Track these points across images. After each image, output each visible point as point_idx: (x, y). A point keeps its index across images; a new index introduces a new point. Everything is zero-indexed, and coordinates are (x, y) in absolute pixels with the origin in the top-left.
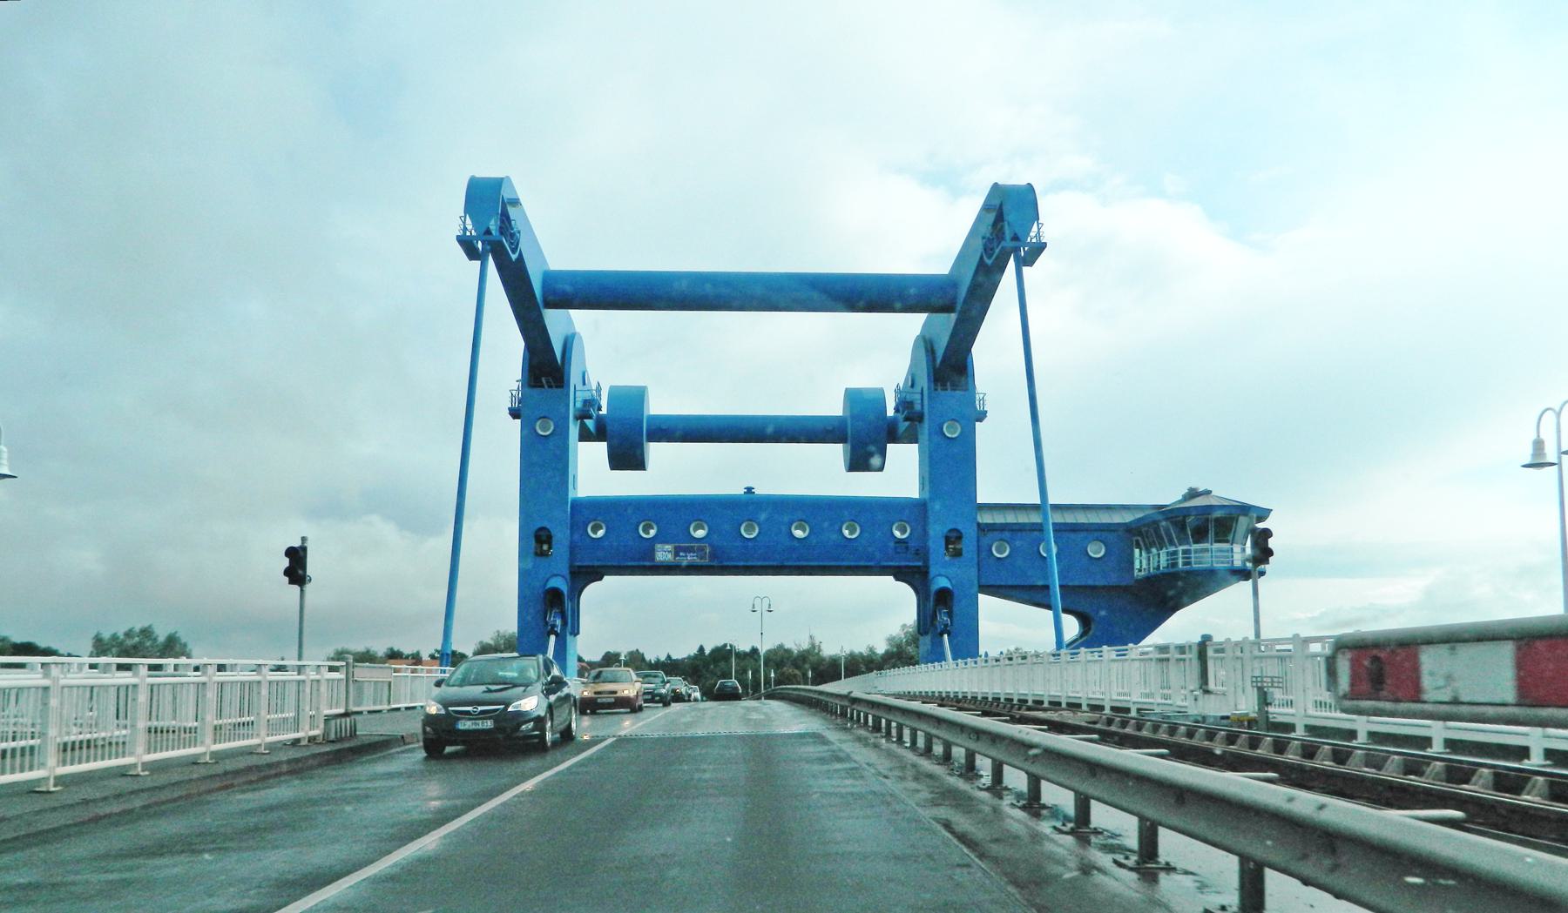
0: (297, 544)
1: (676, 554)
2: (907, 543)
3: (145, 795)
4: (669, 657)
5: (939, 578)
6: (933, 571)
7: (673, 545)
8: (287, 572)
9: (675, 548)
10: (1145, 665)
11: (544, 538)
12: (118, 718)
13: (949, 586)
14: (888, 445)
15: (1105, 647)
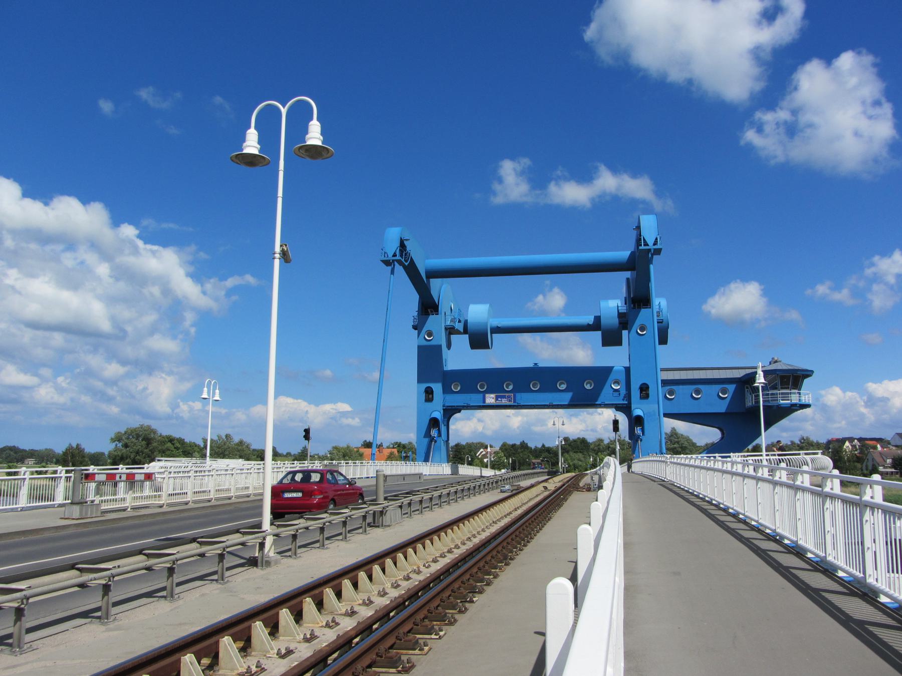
0: (307, 428)
1: (497, 399)
2: (619, 391)
3: (390, 671)
4: (543, 446)
5: (637, 410)
6: (633, 406)
7: (495, 395)
8: (304, 437)
9: (496, 396)
10: (661, 464)
11: (430, 392)
12: (889, 572)
13: (642, 415)
14: (623, 331)
15: (732, 453)
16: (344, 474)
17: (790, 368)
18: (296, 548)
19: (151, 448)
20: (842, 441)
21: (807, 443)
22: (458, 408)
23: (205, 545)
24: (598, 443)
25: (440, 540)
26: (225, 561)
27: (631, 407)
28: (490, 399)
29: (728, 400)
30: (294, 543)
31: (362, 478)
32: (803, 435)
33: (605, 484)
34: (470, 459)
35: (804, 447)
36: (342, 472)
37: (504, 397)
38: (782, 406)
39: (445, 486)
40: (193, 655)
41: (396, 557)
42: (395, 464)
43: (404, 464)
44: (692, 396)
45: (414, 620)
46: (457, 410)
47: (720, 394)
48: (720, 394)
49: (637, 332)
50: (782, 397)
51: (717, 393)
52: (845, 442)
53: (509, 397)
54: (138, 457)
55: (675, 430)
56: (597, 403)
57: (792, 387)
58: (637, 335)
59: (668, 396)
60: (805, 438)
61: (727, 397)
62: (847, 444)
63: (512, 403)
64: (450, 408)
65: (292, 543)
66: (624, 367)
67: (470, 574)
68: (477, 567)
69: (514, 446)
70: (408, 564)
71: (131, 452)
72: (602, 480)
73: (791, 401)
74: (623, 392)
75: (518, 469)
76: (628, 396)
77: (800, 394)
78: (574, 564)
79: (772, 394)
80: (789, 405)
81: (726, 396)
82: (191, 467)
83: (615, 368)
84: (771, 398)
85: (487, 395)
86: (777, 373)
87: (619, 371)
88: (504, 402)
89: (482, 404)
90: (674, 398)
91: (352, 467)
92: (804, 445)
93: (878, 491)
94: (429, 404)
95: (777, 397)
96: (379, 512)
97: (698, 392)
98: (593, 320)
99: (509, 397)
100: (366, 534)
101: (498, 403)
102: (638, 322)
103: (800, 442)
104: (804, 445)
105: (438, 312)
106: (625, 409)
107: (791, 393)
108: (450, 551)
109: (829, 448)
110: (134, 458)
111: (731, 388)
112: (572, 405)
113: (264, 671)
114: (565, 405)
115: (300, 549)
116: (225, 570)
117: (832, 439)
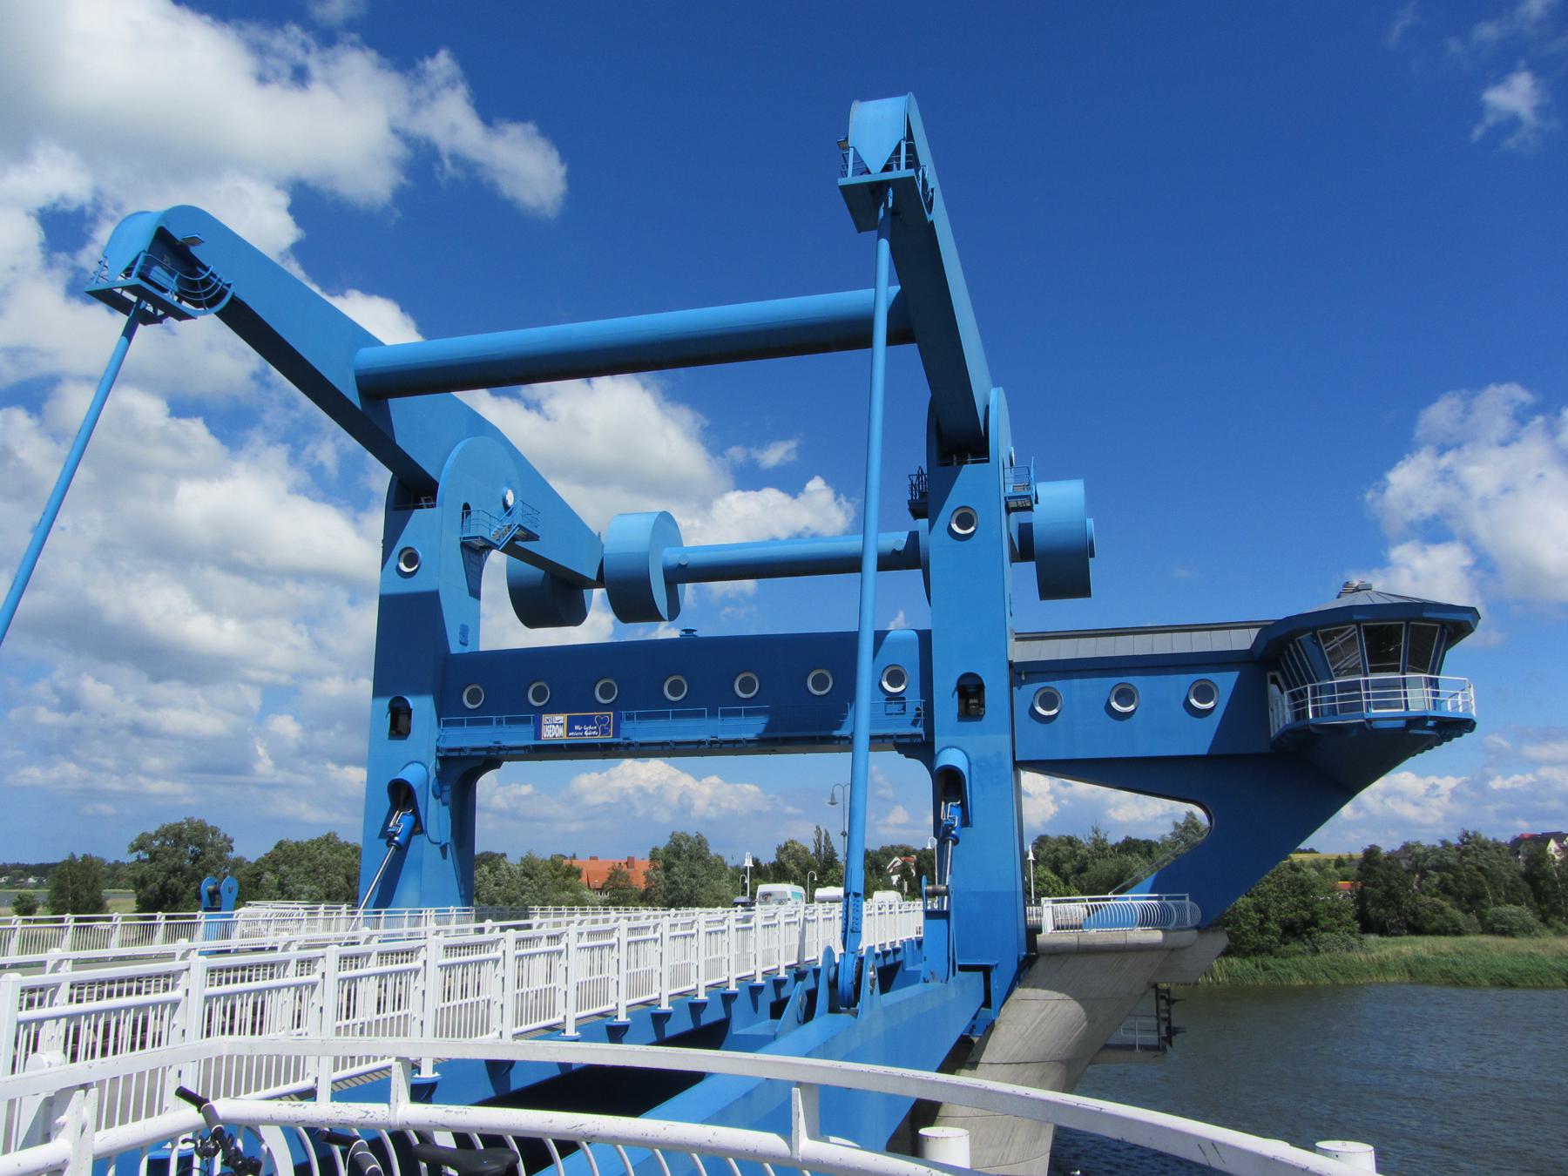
1: (570, 729)
13: (964, 769)
17: (1396, 600)
19: (201, 863)
20: (1545, 838)
21: (1477, 843)
22: (474, 753)
24: (1055, 846)
27: (933, 743)
28: (554, 728)
29: (1215, 720)
32: (1466, 829)
34: (816, 879)
35: (1471, 851)
37: (588, 721)
38: (1379, 725)
44: (1109, 708)
46: (491, 760)
47: (1193, 701)
48: (1193, 701)
49: (950, 530)
50: (1375, 696)
51: (1183, 699)
52: (1549, 841)
53: (602, 721)
54: (173, 880)
55: (1195, 818)
56: (836, 733)
57: (1410, 663)
58: (950, 539)
59: (1039, 709)
60: (1470, 834)
61: (1212, 709)
62: (1552, 845)
63: (609, 739)
64: (456, 754)
66: (917, 631)
69: (1137, 841)
71: (159, 871)
72: (254, 1128)
73: (1407, 708)
74: (914, 700)
75: (87, 999)
76: (927, 714)
77: (1434, 683)
79: (1344, 687)
80: (1401, 723)
81: (1211, 704)
83: (889, 635)
84: (1341, 698)
85: (545, 717)
86: (1356, 617)
87: (901, 643)
88: (590, 734)
89: (532, 742)
90: (1056, 715)
92: (1470, 847)
94: (398, 744)
95: (1359, 697)
97: (1125, 695)
98: (905, 540)
99: (602, 721)
101: (575, 738)
102: (953, 501)
103: (1462, 840)
104: (1470, 847)
105: (435, 499)
106: (920, 748)
107: (1404, 683)
109: (1518, 853)
110: (165, 884)
111: (1225, 682)
112: (768, 743)
114: (749, 741)
117: (1522, 835)
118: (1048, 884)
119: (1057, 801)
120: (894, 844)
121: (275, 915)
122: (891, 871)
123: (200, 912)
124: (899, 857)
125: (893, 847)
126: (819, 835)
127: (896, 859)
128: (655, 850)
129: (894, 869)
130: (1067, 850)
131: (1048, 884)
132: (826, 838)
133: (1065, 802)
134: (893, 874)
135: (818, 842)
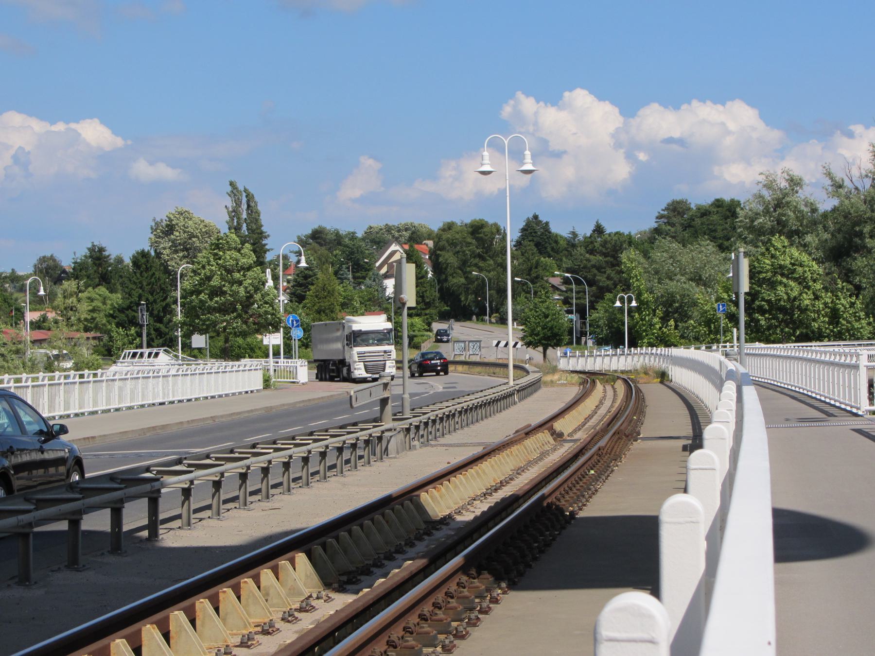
16: (29, 402)
18: (268, 488)
23: (173, 475)
25: (295, 569)
26: (269, 475)
30: (287, 473)
31: (83, 414)
33: (708, 433)
34: (42, 292)
36: (25, 399)
39: (232, 451)
40: (124, 640)
41: (167, 620)
42: (46, 382)
43: (77, 379)
45: (446, 590)
65: (303, 468)
67: (433, 604)
68: (444, 591)
70: (200, 636)
78: (684, 482)
82: (250, 366)
91: (30, 389)
93: (704, 347)
96: (404, 429)
100: (78, 570)
108: (289, 618)
113: (315, 610)
115: (251, 497)
116: (270, 488)
118: (801, 281)
119: (630, 151)
120: (390, 224)
121: (151, 372)
122: (384, 270)
123: (41, 373)
124: (401, 244)
125: (389, 229)
126: (238, 203)
127: (394, 247)
128: (355, 233)
129: (391, 266)
130: (244, 231)
131: (801, 281)
132: (249, 206)
133: (642, 157)
134: (386, 276)
135: (235, 213)
